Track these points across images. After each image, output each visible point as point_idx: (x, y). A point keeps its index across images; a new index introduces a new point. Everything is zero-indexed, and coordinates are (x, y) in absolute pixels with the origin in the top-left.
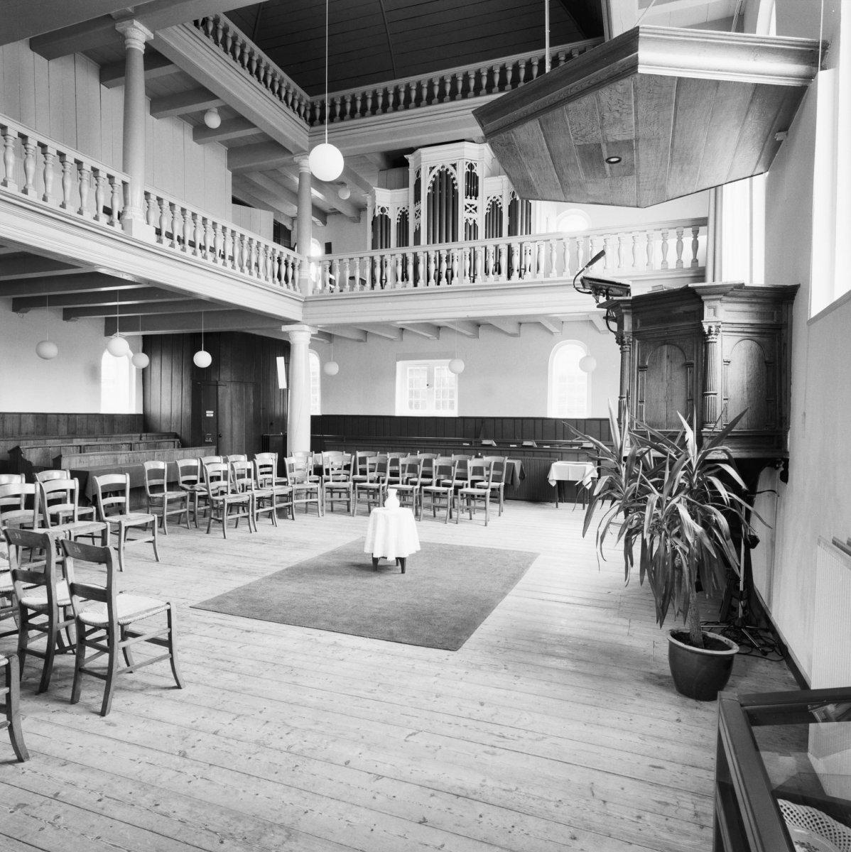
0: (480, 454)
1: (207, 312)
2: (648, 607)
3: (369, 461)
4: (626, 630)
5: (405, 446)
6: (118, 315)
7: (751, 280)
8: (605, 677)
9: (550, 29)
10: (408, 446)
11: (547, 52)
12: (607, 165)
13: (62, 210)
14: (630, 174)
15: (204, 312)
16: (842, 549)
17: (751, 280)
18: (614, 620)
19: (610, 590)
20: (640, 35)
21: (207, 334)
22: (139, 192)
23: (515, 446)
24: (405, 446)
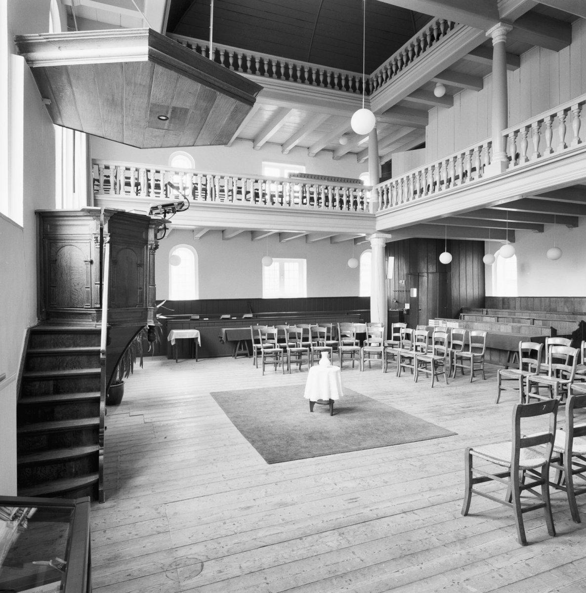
0: (286, 323)
1: (449, 226)
2: (134, 435)
3: (402, 331)
4: (145, 417)
5: (316, 318)
6: (507, 229)
7: (63, 207)
8: (149, 399)
9: (209, 29)
10: (318, 318)
11: (211, 44)
12: (169, 116)
13: (566, 150)
14: (154, 105)
15: (447, 226)
16: (420, 186)
17: (63, 207)
18: (154, 420)
19: (166, 440)
20: (148, 34)
21: (449, 241)
22: (498, 141)
23: (236, 318)
24: (316, 318)
